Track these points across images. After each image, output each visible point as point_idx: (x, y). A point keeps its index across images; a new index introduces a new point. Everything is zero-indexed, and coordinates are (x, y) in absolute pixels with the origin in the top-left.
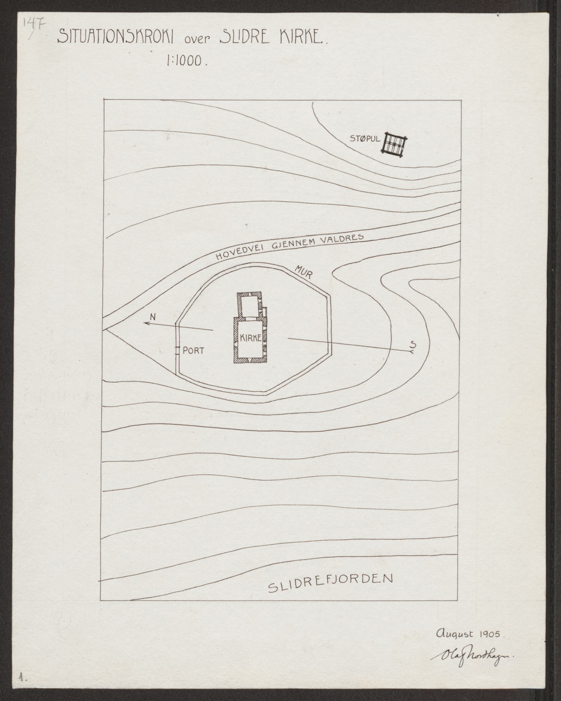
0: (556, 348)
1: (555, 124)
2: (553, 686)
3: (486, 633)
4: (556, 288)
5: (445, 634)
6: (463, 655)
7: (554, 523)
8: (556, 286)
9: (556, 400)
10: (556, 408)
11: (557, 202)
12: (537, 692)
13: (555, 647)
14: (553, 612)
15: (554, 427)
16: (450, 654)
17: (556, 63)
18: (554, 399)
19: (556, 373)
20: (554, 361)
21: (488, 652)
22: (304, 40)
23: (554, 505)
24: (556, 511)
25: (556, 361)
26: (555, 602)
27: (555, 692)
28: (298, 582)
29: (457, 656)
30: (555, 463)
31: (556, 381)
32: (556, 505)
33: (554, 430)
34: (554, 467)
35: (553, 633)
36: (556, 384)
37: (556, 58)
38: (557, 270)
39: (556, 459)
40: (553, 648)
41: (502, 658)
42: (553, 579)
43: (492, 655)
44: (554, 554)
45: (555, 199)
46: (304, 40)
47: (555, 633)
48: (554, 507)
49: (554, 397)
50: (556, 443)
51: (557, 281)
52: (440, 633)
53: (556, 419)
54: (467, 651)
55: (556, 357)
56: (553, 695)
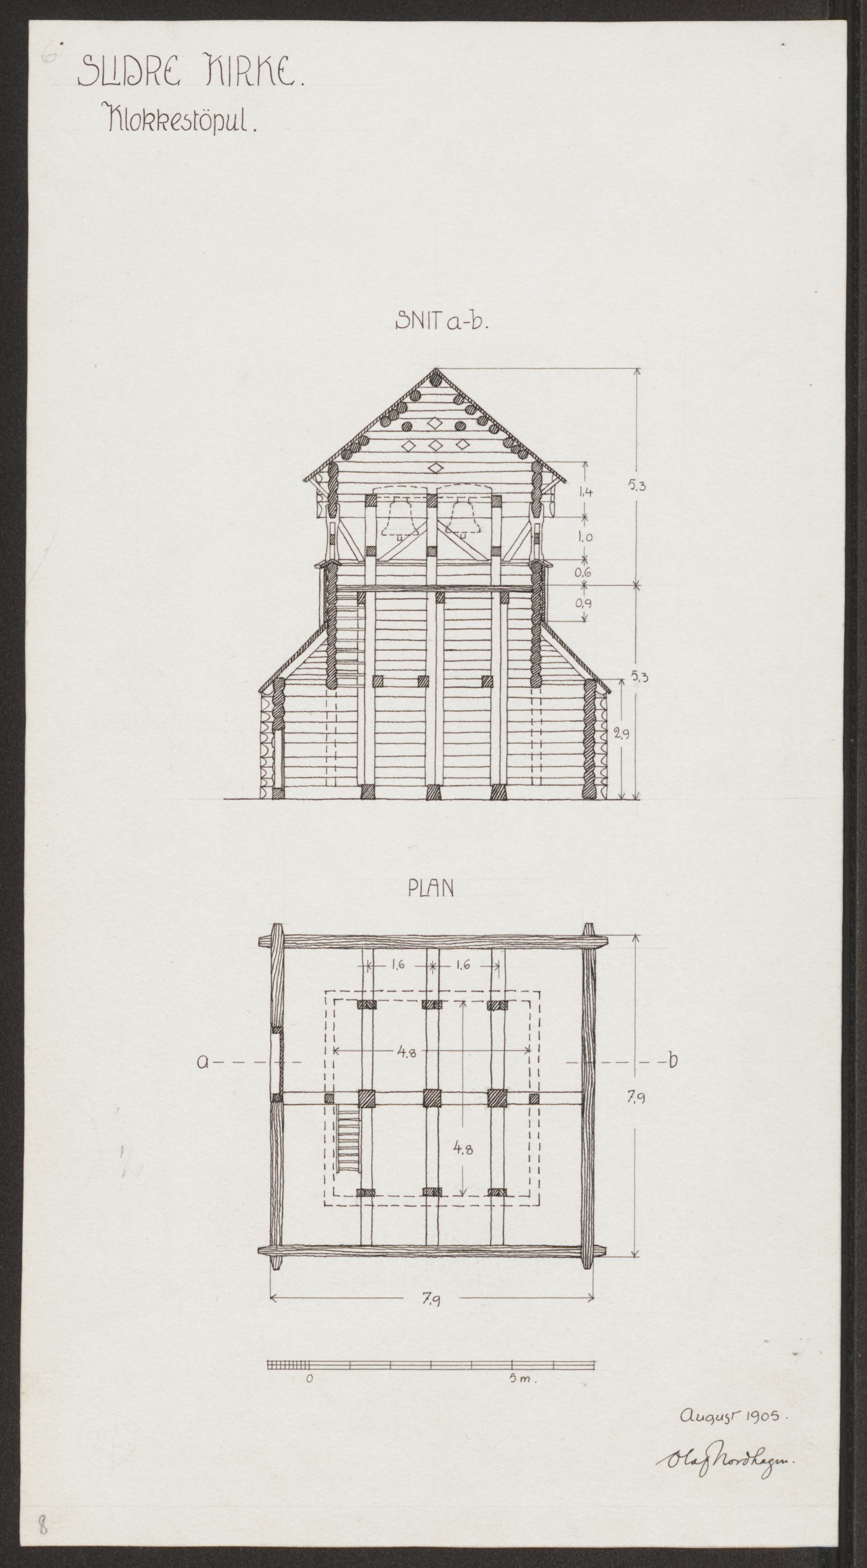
0: (858, 871)
1: (856, 495)
2: (853, 1437)
3: (755, 1414)
4: (858, 772)
5: (694, 1417)
7: (854, 1163)
9: (857, 957)
10: (857, 972)
11: (859, 627)
12: (822, 1552)
13: (856, 1371)
14: (852, 1313)
15: (854, 1003)
16: (682, 1460)
17: (856, 393)
19: (858, 912)
20: (854, 892)
21: (752, 1454)
22: (253, 79)
23: (854, 1133)
24: (857, 1143)
25: (857, 892)
30: (856, 1064)
31: (857, 926)
33: (854, 1007)
34: (854, 1070)
35: (853, 1347)
36: (858, 931)
37: (857, 385)
39: (857, 1057)
40: (853, 1374)
41: (775, 1466)
42: (853, 1257)
43: (691, 1458)
44: (853, 1216)
45: (856, 621)
47: (856, 1348)
49: (854, 953)
50: (857, 1030)
52: (686, 1416)
53: (857, 989)
54: (713, 1454)
55: (858, 887)
56: (853, 1451)
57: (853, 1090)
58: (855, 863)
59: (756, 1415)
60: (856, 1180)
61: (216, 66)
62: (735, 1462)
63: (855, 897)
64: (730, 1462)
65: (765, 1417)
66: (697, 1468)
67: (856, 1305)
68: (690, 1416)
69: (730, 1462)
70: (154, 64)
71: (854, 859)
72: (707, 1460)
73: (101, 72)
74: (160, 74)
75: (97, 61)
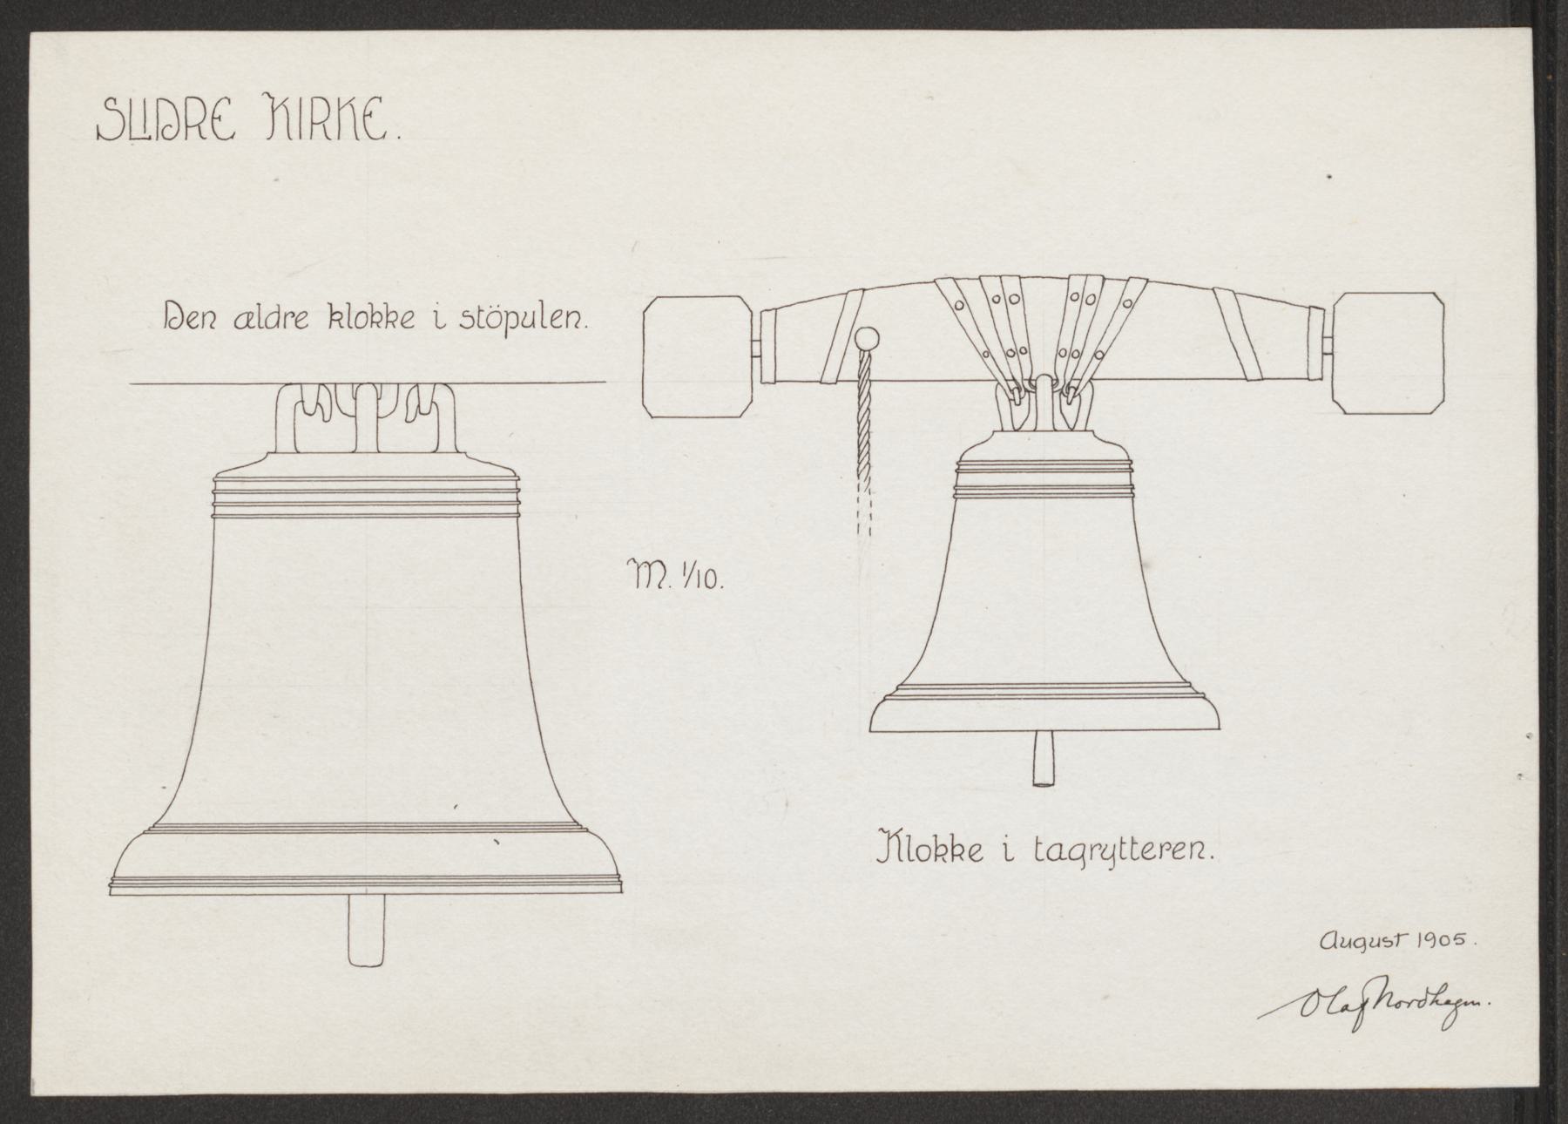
2: (1555, 1071)
4: (1558, 121)
6: (1363, 1006)
8: (1558, 114)
12: (1519, 1093)
13: (1559, 977)
15: (1553, 451)
16: (1325, 1002)
18: (1554, 386)
19: (1558, 323)
20: (1554, 294)
22: (333, 134)
25: (1558, 293)
26: (1559, 869)
27: (1560, 1085)
28: (512, 316)
29: (1345, 1008)
30: (1558, 539)
32: (1560, 636)
33: (1554, 458)
35: (1554, 942)
38: (1559, 78)
40: (1554, 981)
43: (1442, 998)
46: (333, 134)
48: (1554, 642)
50: (1558, 491)
51: (1559, 104)
54: (1373, 993)
55: (1558, 286)
57: (1554, 576)
58: (1554, 252)
59: (1431, 938)
60: (1559, 704)
61: (280, 113)
62: (1404, 1005)
63: (1554, 300)
64: (1397, 1005)
65: (1445, 941)
66: (1350, 1017)
67: (1559, 882)
68: (1335, 942)
69: (1397, 1005)
70: (195, 114)
71: (1552, 245)
72: (1363, 1006)
73: (126, 125)
74: (206, 127)
75: (123, 106)
